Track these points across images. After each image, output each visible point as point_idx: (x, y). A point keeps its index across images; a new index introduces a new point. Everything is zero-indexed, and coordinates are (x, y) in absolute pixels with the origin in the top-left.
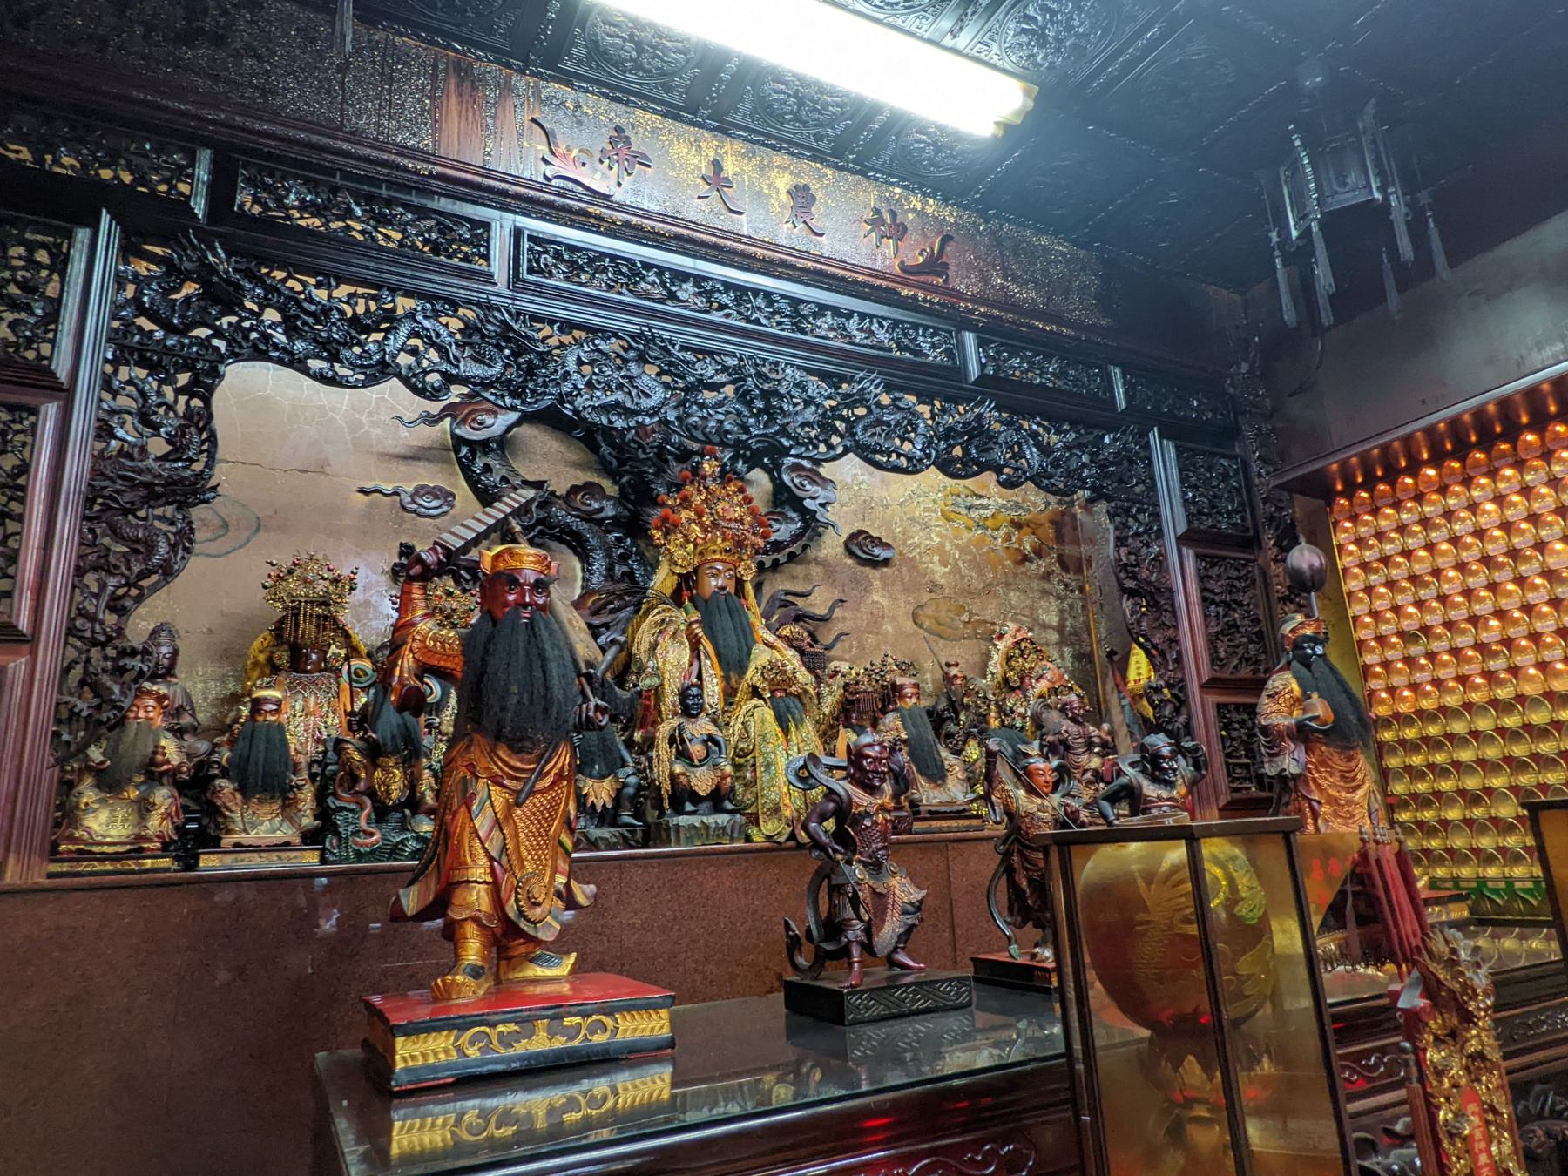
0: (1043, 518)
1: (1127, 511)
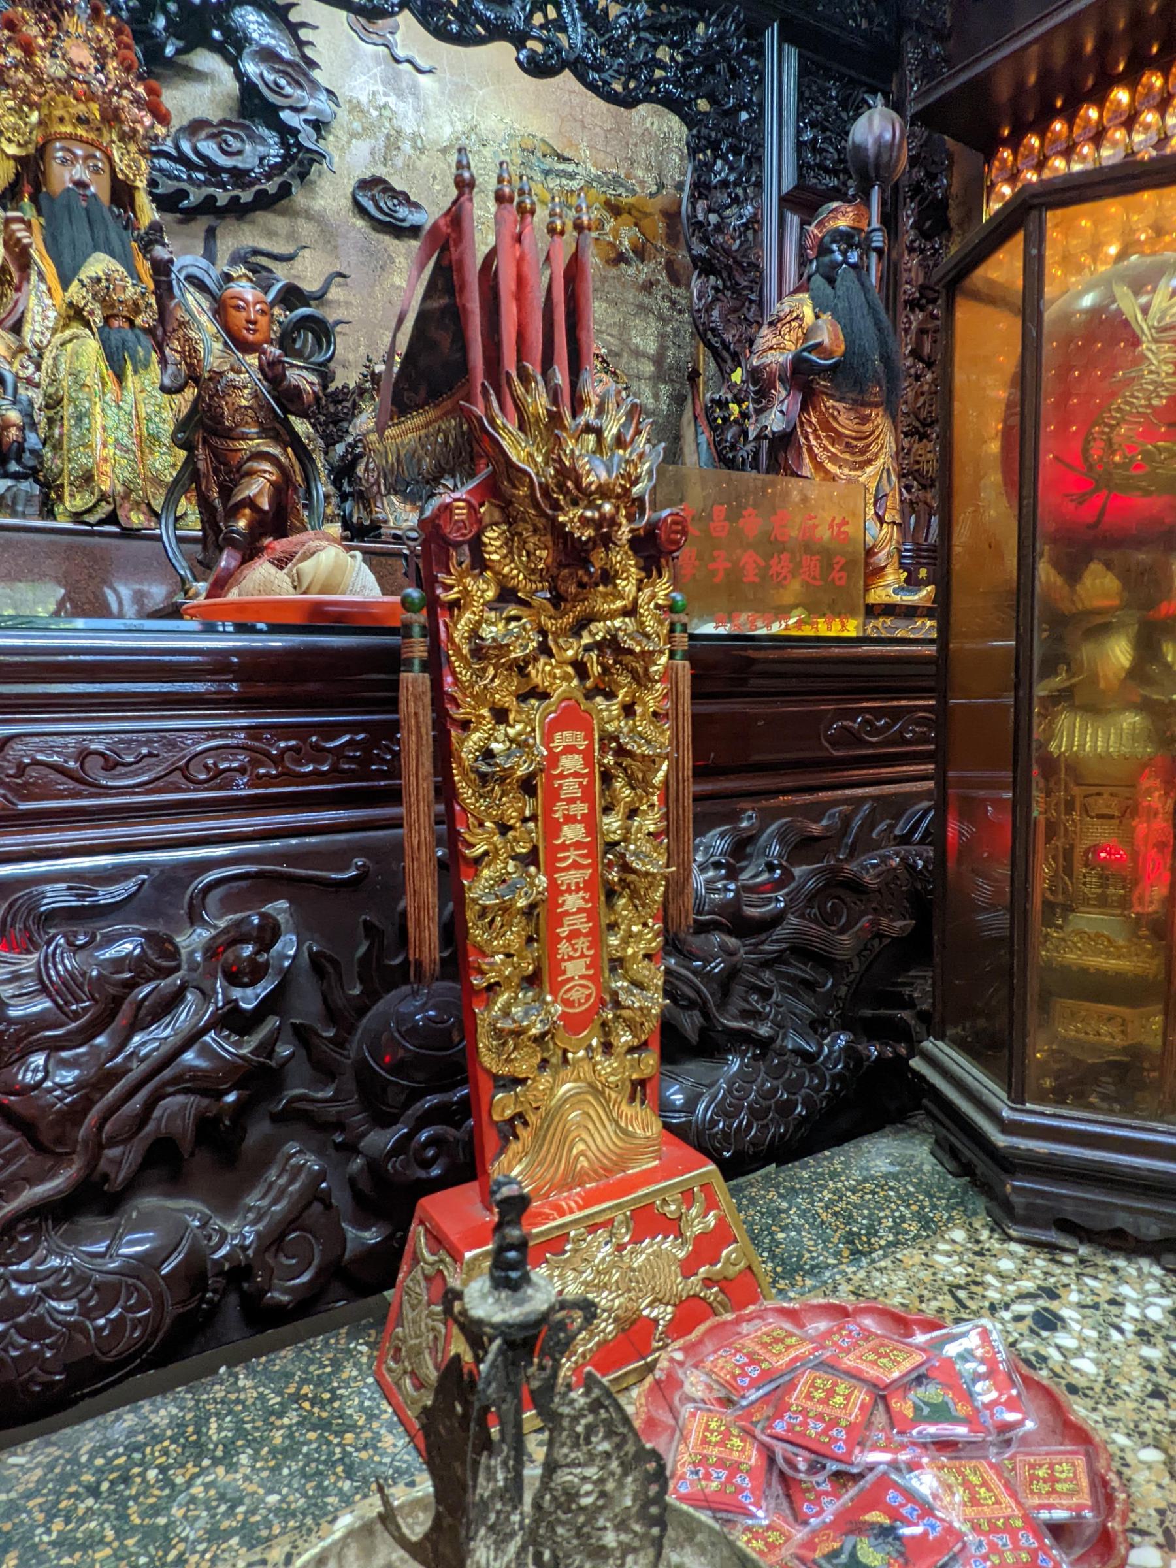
0: (654, 206)
1: (715, 146)
